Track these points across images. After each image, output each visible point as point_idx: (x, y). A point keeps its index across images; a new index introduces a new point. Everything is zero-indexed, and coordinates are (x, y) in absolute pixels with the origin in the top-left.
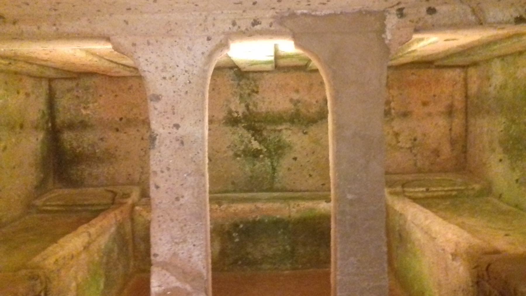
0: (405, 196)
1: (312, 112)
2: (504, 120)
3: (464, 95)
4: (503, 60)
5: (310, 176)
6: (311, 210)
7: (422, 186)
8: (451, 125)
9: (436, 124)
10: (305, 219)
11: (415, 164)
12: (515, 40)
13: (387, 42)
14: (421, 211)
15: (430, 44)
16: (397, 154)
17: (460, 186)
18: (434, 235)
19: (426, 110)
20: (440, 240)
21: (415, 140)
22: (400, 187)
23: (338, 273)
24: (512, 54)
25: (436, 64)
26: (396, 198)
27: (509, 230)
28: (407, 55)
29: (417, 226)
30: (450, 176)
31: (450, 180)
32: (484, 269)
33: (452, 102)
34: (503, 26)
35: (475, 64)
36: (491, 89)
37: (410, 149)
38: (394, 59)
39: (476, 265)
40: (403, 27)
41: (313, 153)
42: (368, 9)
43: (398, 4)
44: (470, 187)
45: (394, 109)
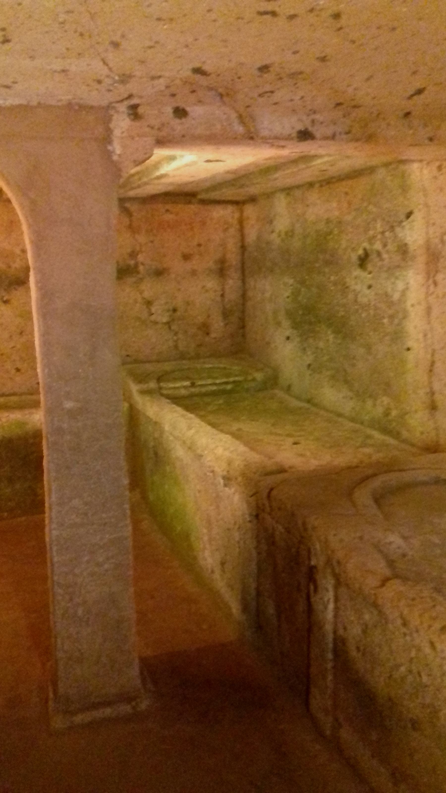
0: (162, 395)
1: (16, 268)
2: (291, 281)
3: (240, 244)
4: (288, 194)
5: (18, 370)
6: (21, 424)
7: (187, 378)
8: (223, 289)
9: (203, 287)
10: (10, 441)
11: (176, 347)
12: (302, 166)
13: (115, 158)
14: (183, 416)
15: (186, 165)
16: (150, 332)
17: (236, 376)
18: (199, 452)
19: (188, 266)
20: (209, 459)
21: (175, 310)
22: (155, 381)
23: (54, 526)
24: (298, 187)
25: (199, 197)
26: (147, 398)
27: (300, 436)
28: (156, 182)
29: (176, 438)
30: (224, 363)
31: (225, 368)
32: (265, 494)
33: (224, 255)
34: (282, 143)
35: (253, 200)
36: (274, 236)
37: (168, 323)
38: (139, 186)
39: (254, 491)
40: (138, 135)
41: (21, 333)
42: (82, 102)
43: (130, 97)
44: (250, 378)
45: (143, 264)
